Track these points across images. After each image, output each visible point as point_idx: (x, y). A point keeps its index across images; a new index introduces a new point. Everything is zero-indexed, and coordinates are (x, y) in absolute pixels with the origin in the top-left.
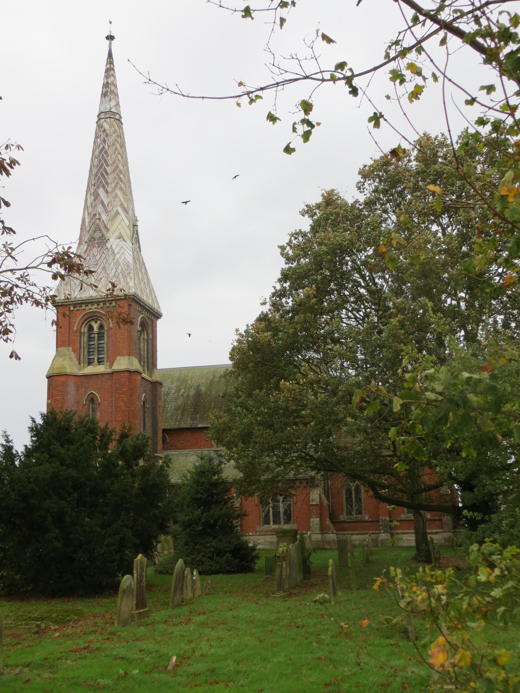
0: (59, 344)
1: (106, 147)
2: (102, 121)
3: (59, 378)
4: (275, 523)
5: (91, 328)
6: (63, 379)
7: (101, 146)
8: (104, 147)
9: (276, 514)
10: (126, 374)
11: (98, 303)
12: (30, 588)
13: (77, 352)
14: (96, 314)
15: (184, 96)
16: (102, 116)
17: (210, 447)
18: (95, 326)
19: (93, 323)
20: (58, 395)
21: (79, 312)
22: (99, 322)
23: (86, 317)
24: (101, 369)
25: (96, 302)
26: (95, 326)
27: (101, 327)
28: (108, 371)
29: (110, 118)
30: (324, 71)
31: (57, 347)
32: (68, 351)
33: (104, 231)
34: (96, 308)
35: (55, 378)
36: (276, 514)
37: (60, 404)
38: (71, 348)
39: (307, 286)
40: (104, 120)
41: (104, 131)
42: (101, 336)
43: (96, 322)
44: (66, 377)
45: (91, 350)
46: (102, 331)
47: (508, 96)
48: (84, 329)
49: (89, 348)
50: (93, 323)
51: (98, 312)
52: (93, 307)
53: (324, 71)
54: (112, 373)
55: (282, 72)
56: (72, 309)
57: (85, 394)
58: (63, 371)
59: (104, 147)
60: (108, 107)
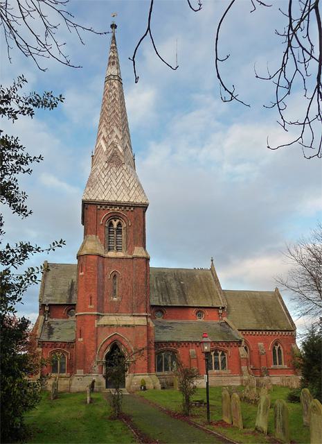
4: (216, 369)
5: (111, 224)
7: (113, 98)
8: (115, 99)
9: (217, 363)
11: (120, 207)
15: (282, 118)
16: (112, 77)
18: (115, 224)
19: (113, 221)
22: (118, 221)
25: (118, 206)
26: (115, 224)
27: (119, 224)
30: (230, 93)
31: (85, 234)
36: (217, 363)
39: (9, 299)
41: (114, 88)
42: (119, 231)
46: (120, 228)
51: (120, 213)
52: (116, 209)
53: (230, 93)
55: (307, 121)
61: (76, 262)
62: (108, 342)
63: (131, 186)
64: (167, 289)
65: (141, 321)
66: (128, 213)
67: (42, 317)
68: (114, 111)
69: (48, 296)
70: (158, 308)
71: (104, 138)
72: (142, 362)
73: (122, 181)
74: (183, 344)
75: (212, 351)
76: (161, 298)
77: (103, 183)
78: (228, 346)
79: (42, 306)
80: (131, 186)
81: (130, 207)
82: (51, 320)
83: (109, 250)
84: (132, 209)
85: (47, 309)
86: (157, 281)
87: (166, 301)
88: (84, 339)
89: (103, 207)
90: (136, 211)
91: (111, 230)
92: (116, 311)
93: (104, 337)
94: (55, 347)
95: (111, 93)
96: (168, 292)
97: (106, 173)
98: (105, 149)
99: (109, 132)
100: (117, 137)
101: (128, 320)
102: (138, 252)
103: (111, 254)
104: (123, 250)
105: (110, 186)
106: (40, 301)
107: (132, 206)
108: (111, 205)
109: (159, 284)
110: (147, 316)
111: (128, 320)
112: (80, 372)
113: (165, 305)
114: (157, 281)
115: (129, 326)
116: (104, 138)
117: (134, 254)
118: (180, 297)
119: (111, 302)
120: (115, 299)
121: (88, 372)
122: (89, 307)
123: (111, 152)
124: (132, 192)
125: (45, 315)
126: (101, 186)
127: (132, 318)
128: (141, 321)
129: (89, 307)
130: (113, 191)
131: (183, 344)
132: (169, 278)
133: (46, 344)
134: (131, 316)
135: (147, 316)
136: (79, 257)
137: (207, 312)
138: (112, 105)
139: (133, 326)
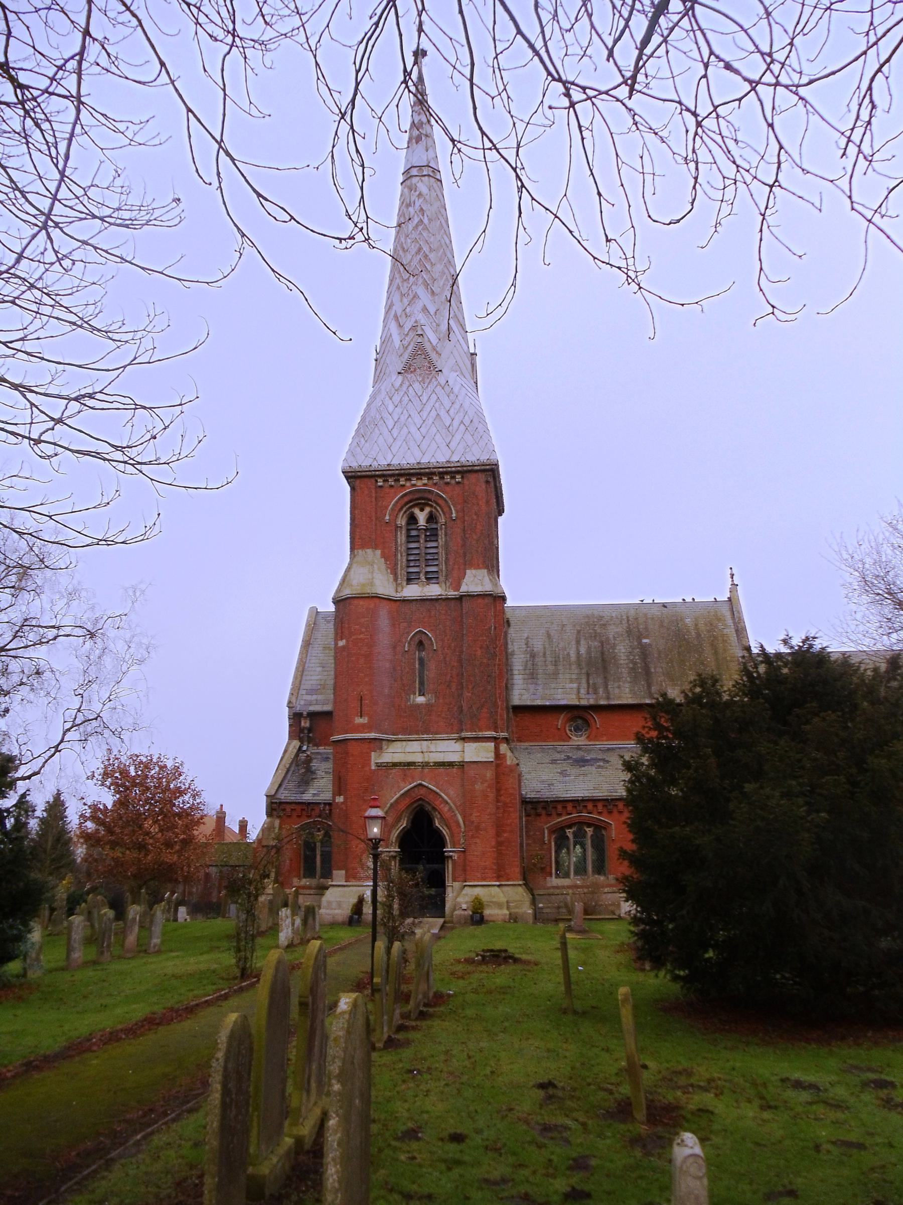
0: (356, 543)
1: (426, 221)
2: (415, 180)
3: (361, 602)
4: (557, 876)
5: (412, 519)
6: (371, 604)
7: (416, 220)
8: (421, 221)
10: (490, 600)
12: (682, 973)
13: (390, 559)
14: (426, 495)
16: (414, 172)
17: (564, 740)
18: (422, 517)
19: (417, 511)
20: (362, 633)
21: (393, 490)
23: (406, 499)
24: (434, 590)
26: (422, 517)
27: (431, 518)
28: (452, 593)
29: (429, 175)
31: (352, 549)
32: (374, 555)
33: (433, 356)
34: (425, 485)
35: (356, 602)
37: (365, 649)
38: (379, 552)
40: (418, 178)
41: (420, 195)
43: (422, 510)
44: (377, 601)
45: (412, 558)
47: (228, 47)
48: (402, 521)
49: (408, 555)
50: (417, 511)
51: (430, 491)
54: (460, 599)
56: (380, 484)
57: (408, 633)
58: (368, 590)
59: (421, 221)
60: (425, 159)
61: (332, 608)
62: (402, 806)
63: (456, 423)
64: (603, 660)
65: (479, 752)
66: (448, 489)
67: (296, 743)
68: (420, 249)
69: (310, 692)
70: (576, 713)
71: (396, 318)
72: (482, 849)
73: (434, 413)
74: (559, 807)
75: (570, 827)
76: (584, 684)
77: (390, 423)
78: (610, 812)
79: (296, 717)
80: (456, 423)
81: (453, 474)
82: (314, 750)
83: (409, 581)
84: (458, 478)
85: (305, 724)
86: (578, 642)
87: (596, 692)
88: (345, 799)
89: (391, 482)
90: (466, 481)
91: (414, 533)
92: (418, 725)
93: (395, 792)
94: (309, 817)
95: (411, 209)
96: (605, 669)
97: (396, 398)
98: (397, 343)
99: (406, 301)
100: (425, 309)
101: (447, 750)
102: (474, 582)
103: (412, 591)
104: (442, 579)
105: (405, 430)
106: (290, 705)
107: (458, 472)
108: (407, 474)
109: (583, 650)
110: (495, 739)
111: (447, 750)
112: (339, 876)
113: (592, 702)
114: (578, 642)
115: (451, 764)
116: (396, 316)
117: (464, 588)
118: (635, 680)
119: (412, 706)
120: (421, 700)
121: (351, 876)
122: (359, 720)
123: (410, 348)
124: (458, 437)
125: (301, 740)
126: (386, 432)
127: (457, 746)
128: (479, 752)
129: (359, 720)
130: (419, 444)
131: (559, 807)
132: (612, 631)
133: (288, 810)
134: (457, 740)
135: (495, 739)
136: (337, 602)
137: (597, 720)
138: (414, 235)
139: (462, 765)
